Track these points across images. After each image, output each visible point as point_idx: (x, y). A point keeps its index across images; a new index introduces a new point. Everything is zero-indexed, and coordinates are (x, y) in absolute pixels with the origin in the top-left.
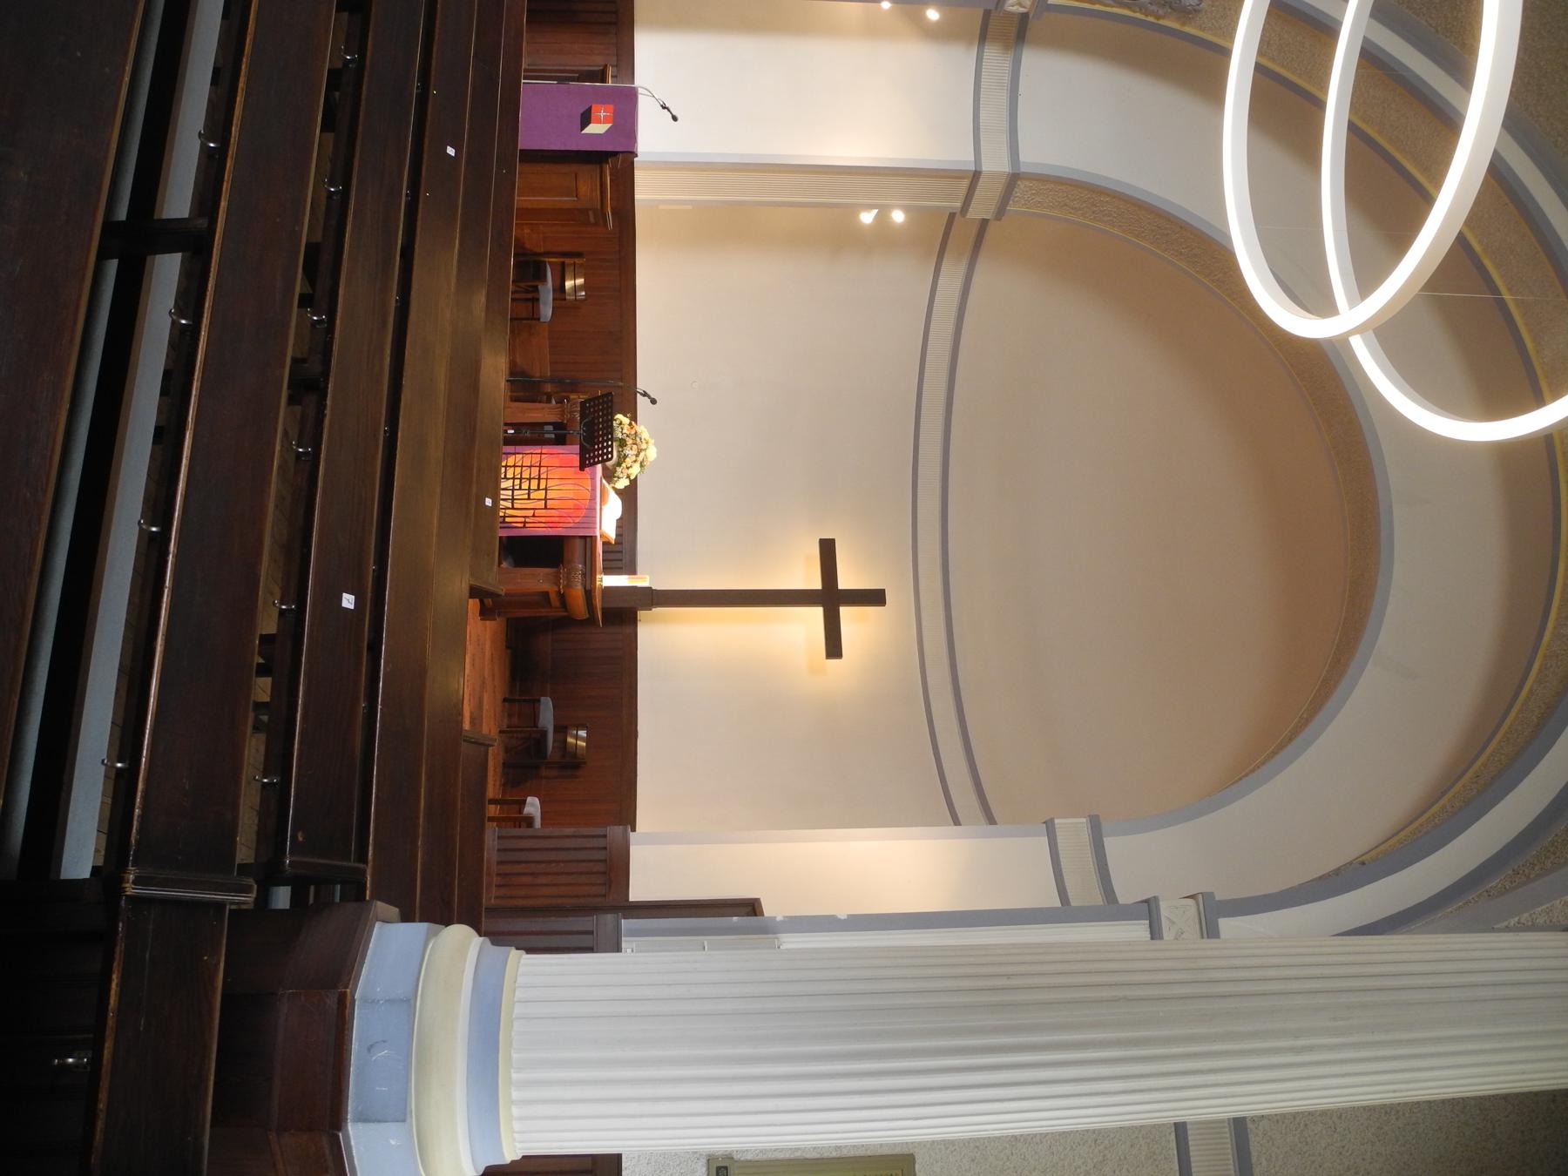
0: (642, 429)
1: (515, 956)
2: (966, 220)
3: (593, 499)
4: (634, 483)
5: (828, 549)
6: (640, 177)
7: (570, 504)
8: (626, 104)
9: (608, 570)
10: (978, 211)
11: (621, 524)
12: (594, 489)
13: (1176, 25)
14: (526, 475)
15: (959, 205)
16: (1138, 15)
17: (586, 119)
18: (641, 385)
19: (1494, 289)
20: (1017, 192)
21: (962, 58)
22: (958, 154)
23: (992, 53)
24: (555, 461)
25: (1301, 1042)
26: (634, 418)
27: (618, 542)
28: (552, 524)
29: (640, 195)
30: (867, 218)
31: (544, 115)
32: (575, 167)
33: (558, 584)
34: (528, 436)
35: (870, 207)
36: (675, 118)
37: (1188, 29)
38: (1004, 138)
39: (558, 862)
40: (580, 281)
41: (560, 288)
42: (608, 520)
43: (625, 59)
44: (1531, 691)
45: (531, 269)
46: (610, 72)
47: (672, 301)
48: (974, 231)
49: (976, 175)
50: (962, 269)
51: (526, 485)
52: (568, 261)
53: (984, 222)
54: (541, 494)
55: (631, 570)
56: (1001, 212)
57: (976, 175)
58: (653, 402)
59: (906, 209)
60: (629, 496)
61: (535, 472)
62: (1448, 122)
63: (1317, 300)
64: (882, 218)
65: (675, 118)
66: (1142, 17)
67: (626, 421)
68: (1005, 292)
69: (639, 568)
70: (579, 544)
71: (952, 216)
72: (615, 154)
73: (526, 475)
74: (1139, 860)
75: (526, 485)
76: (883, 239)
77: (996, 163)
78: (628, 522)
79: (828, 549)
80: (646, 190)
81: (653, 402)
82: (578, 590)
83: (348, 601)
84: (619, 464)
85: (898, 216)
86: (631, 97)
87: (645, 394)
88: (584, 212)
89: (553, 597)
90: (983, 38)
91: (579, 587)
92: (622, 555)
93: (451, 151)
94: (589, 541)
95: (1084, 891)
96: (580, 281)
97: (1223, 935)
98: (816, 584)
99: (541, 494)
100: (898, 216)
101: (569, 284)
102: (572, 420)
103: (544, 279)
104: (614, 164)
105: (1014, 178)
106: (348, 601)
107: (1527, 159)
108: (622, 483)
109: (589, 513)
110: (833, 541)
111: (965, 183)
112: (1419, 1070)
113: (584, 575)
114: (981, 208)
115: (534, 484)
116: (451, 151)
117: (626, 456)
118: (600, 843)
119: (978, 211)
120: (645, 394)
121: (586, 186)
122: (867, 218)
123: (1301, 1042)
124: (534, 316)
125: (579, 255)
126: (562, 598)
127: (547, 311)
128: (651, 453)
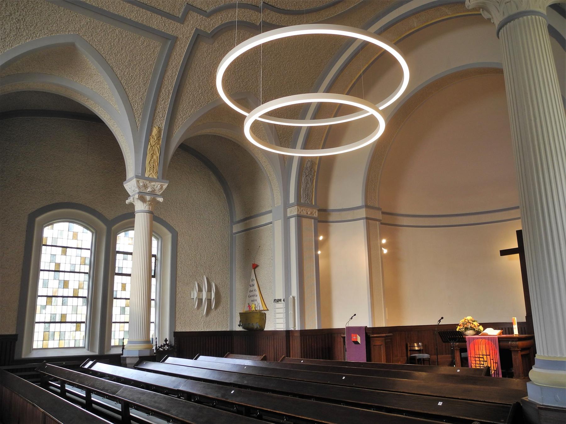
0: (461, 322)
1: (537, 357)
2: (382, 219)
3: (485, 338)
4: (480, 324)
5: (504, 253)
6: (377, 325)
7: (487, 346)
8: (352, 330)
9: (513, 333)
11: (495, 329)
12: (482, 338)
13: (317, 166)
14: (478, 362)
17: (356, 343)
18: (436, 323)
19: (360, 76)
21: (334, 228)
22: (361, 225)
23: (331, 219)
24: (473, 352)
25: (532, 118)
26: (458, 325)
27: (502, 329)
28: (495, 354)
29: (383, 325)
30: (385, 251)
31: (356, 354)
32: (372, 346)
33: (517, 351)
34: (465, 362)
35: (382, 251)
36: (355, 315)
37: (317, 162)
38: (356, 211)
40: (416, 345)
41: (419, 351)
42: (492, 332)
45: (412, 360)
46: (343, 335)
47: (419, 313)
49: (367, 218)
50: (401, 218)
51: (482, 363)
52: (409, 349)
54: (485, 357)
55: (512, 324)
56: (378, 209)
58: (442, 318)
59: (381, 239)
60: (486, 326)
61: (477, 359)
62: (366, 44)
63: (371, 123)
64: (385, 246)
65: (355, 315)
67: (459, 327)
68: (406, 204)
69: (511, 321)
70: (504, 344)
71: (382, 224)
72: (366, 333)
73: (478, 362)
75: (482, 363)
76: (392, 245)
77: (362, 213)
78: (495, 326)
79: (504, 253)
80: (382, 323)
81: (442, 318)
82: (520, 343)
83: (440, 404)
84: (474, 329)
85: (384, 241)
86: (348, 328)
87: (440, 321)
88: (386, 343)
89: (523, 353)
90: (327, 222)
91: (517, 343)
92: (506, 327)
93: (344, 378)
94: (500, 340)
96: (416, 345)
98: (517, 255)
99: (485, 357)
100: (384, 241)
101: (417, 348)
102: (458, 346)
103: (415, 356)
104: (370, 334)
105: (367, 206)
106: (440, 404)
108: (481, 328)
109: (490, 339)
110: (501, 251)
111: (370, 221)
112: (539, 81)
113: (513, 341)
114: (378, 215)
115: (482, 359)
116: (344, 378)
117: (471, 327)
119: (379, 216)
120: (440, 321)
121: (378, 342)
122: (385, 251)
123: (532, 118)
124: (428, 360)
125: (407, 345)
126: (523, 349)
127: (426, 356)
128: (469, 318)
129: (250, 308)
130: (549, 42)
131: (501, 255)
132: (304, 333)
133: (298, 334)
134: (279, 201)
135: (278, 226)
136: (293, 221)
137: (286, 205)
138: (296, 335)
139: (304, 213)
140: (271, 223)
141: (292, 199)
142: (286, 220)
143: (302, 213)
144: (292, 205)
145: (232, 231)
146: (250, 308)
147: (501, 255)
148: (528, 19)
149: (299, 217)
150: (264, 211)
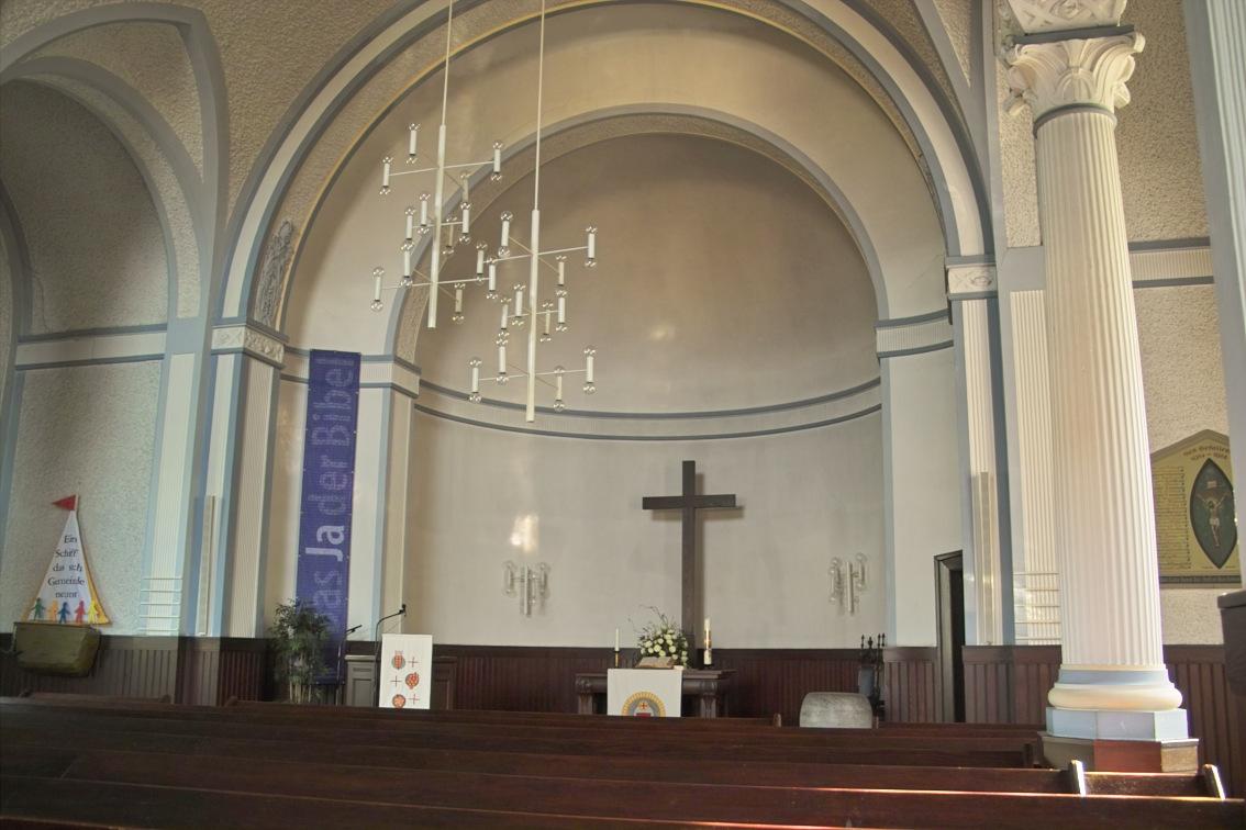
10: (415, 388)
15: (410, 400)
16: (290, 267)
20: (403, 357)
26: (602, 659)
37: (302, 233)
39: (909, 697)
43: (199, 638)
44: (799, 33)
48: (546, 416)
53: (423, 383)
57: (394, 387)
66: (291, 264)
74: (900, 292)
95: (934, 333)
97: (1211, 274)
107: (876, 31)
110: (693, 462)
111: (398, 395)
118: (895, 667)
119: (415, 388)
129: (63, 617)
130: (992, 179)
131: (685, 463)
132: (228, 645)
133: (216, 648)
134: (191, 301)
135: (184, 368)
136: (227, 367)
137: (216, 319)
138: (204, 647)
139: (256, 349)
140: (160, 357)
141: (232, 307)
142: (211, 357)
143: (252, 349)
144: (231, 322)
145: (12, 358)
146: (63, 617)
147: (685, 463)
148: (1076, 119)
149: (247, 355)
150: (134, 322)
